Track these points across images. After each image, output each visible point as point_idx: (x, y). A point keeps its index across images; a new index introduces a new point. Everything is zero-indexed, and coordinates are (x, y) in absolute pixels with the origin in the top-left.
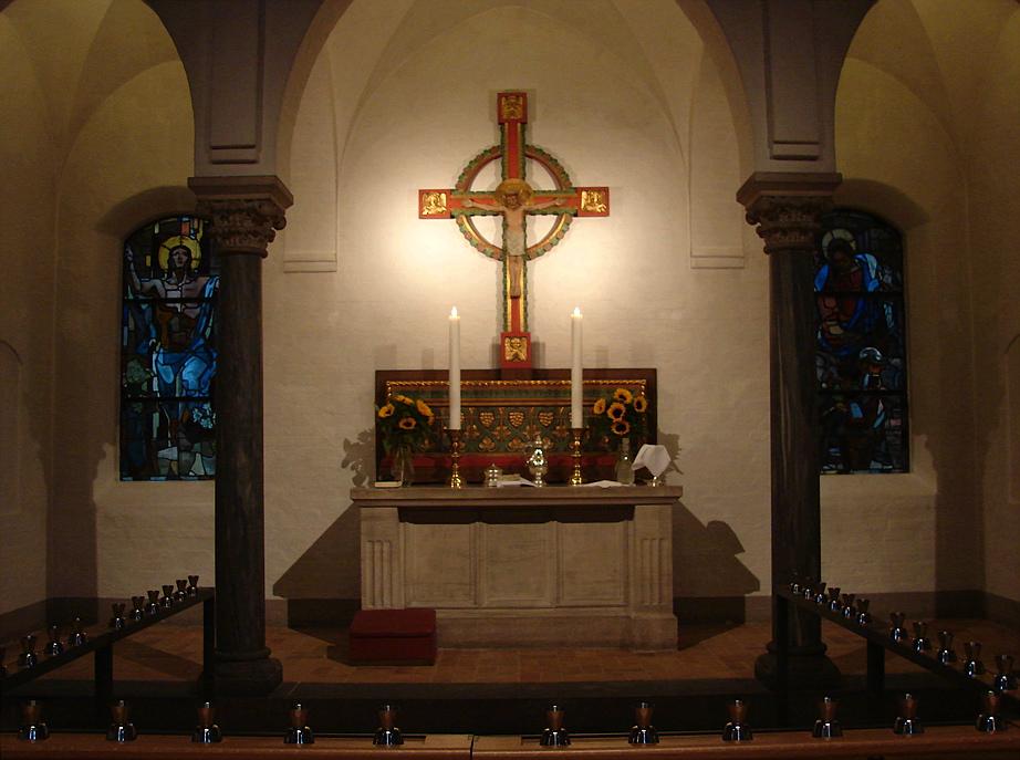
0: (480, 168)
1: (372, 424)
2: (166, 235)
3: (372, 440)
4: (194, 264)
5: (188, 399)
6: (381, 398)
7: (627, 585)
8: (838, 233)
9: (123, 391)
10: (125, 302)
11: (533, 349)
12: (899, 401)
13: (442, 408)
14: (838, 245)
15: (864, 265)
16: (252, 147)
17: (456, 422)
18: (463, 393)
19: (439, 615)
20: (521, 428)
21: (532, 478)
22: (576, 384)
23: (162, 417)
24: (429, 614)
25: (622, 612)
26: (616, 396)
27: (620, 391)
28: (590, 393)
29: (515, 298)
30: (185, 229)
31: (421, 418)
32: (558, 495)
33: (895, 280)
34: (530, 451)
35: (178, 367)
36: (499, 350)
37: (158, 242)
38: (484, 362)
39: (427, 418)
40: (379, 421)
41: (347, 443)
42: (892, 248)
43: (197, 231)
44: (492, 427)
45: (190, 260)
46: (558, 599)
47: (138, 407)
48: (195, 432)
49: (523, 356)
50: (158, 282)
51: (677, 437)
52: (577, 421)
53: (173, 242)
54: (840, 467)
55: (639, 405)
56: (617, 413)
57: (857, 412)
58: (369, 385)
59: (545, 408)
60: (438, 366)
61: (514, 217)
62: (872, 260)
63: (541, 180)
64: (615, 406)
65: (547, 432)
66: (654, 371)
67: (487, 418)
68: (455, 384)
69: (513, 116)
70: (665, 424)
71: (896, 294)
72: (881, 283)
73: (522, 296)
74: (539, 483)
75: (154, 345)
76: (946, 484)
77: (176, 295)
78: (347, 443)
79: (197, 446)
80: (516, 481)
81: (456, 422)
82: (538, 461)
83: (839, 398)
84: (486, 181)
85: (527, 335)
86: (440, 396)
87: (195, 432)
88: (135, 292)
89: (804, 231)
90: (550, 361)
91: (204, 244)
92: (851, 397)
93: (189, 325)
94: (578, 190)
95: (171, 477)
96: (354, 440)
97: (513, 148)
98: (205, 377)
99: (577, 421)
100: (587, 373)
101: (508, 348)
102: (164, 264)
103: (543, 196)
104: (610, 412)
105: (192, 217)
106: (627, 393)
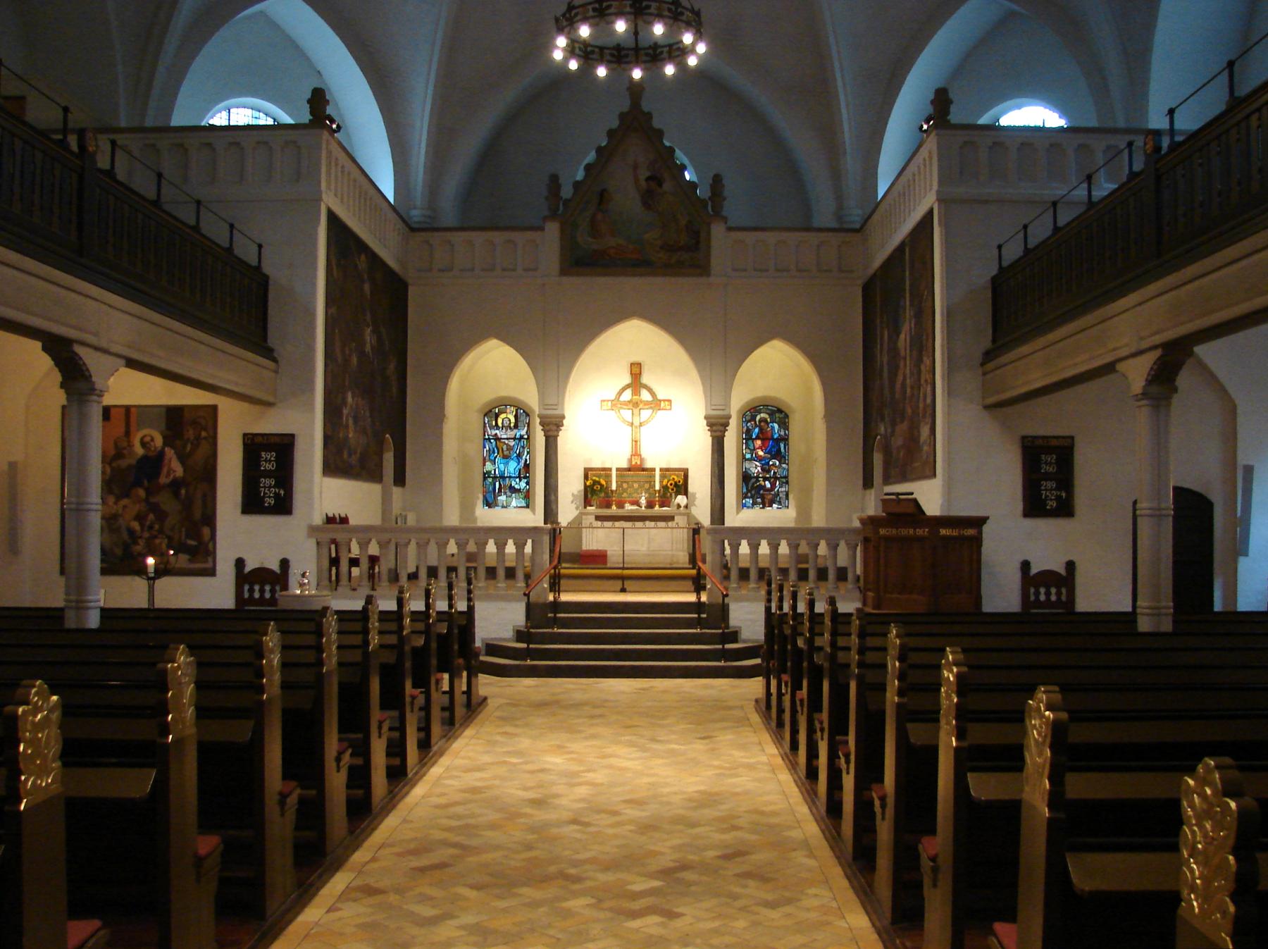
0: (623, 391)
1: (583, 488)
2: (501, 412)
3: (583, 493)
4: (512, 425)
5: (510, 477)
6: (586, 477)
7: (672, 544)
8: (762, 415)
9: (484, 474)
10: (485, 439)
11: (642, 460)
12: (785, 480)
13: (609, 482)
14: (762, 420)
15: (773, 428)
16: (556, 405)
17: (614, 487)
18: (617, 476)
19: (608, 553)
20: (638, 489)
21: (641, 507)
22: (658, 473)
23: (500, 485)
24: (606, 551)
25: (670, 553)
26: (671, 478)
27: (673, 476)
28: (663, 477)
29: (636, 441)
30: (508, 411)
31: (602, 486)
32: (650, 512)
33: (785, 433)
34: (640, 498)
35: (506, 464)
36: (630, 460)
37: (497, 416)
38: (625, 465)
39: (603, 485)
40: (586, 487)
41: (573, 494)
42: (784, 424)
43: (513, 412)
44: (627, 489)
45: (510, 423)
46: (649, 548)
47: (490, 480)
48: (513, 490)
49: (639, 463)
50: (497, 432)
51: (696, 494)
52: (657, 487)
53: (503, 416)
54: (761, 506)
55: (679, 482)
56: (671, 484)
57: (768, 485)
58: (581, 473)
59: (647, 482)
60: (607, 466)
61: (636, 411)
62: (776, 426)
63: (645, 396)
64: (670, 482)
65: (647, 491)
66: (687, 469)
67: (625, 486)
68: (614, 473)
69: (636, 371)
70: (691, 489)
71: (785, 439)
72: (780, 435)
73: (646, 51)
74: (643, 508)
75: (496, 456)
76: (799, 513)
77: (505, 437)
78: (573, 494)
79: (514, 495)
80: (635, 507)
81: (614, 487)
82: (643, 501)
83: (761, 479)
84: (627, 395)
85: (640, 455)
86: (608, 477)
87: (513, 490)
88: (488, 435)
89: (721, 431)
90: (648, 465)
91: (516, 417)
92: (765, 479)
93: (510, 448)
94: (660, 401)
95: (503, 507)
96: (576, 493)
97: (636, 382)
98: (517, 469)
99: (657, 487)
100: (661, 470)
101: (633, 459)
102: (500, 424)
103: (647, 403)
104: (669, 485)
105: (511, 406)
106: (675, 477)
